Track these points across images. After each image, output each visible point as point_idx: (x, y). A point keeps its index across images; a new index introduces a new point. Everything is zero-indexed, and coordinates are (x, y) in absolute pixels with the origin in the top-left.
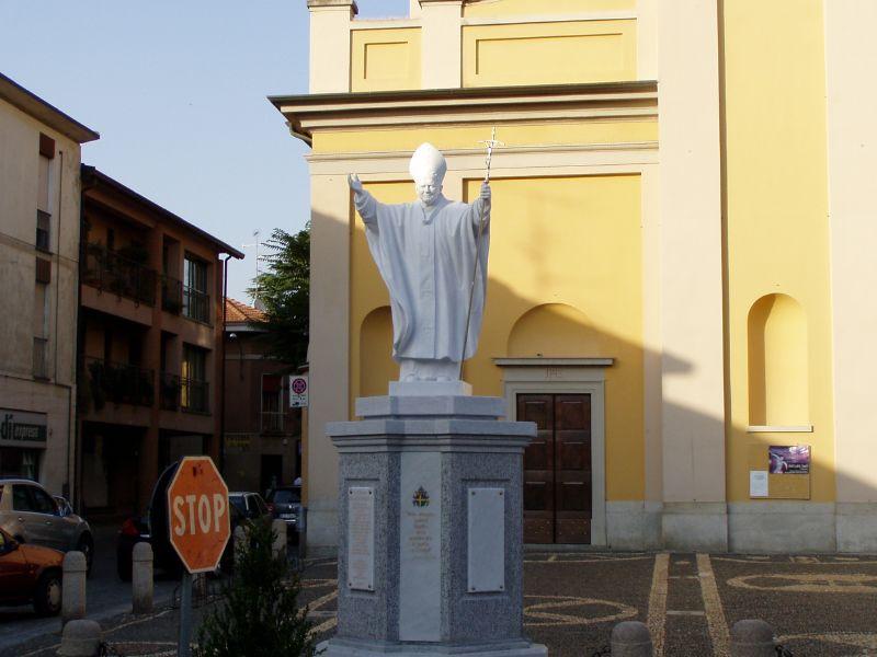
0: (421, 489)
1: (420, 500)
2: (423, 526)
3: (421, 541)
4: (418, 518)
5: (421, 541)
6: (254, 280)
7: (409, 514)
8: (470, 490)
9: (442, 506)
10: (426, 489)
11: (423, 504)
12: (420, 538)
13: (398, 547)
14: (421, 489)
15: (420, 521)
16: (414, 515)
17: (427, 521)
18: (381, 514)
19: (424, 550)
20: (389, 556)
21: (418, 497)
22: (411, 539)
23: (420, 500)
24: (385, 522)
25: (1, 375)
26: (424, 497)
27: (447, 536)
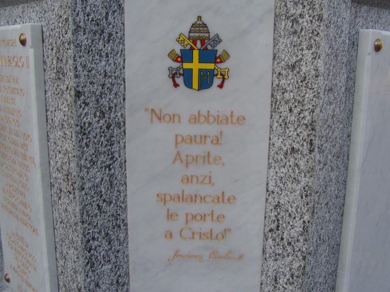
0: (199, 26)
1: (195, 66)
2: (207, 158)
3: (197, 208)
4: (186, 129)
5: (197, 208)
6: (161, 122)
7: (157, 116)
8: (369, 36)
9: (276, 89)
10: (215, 27)
11: (206, 80)
12: (193, 199)
13: (119, 222)
14: (199, 26)
15: (192, 140)
16: (173, 118)
17: (217, 141)
18: (59, 116)
19: (210, 235)
20: (90, 263)
21: (185, 56)
22: (163, 198)
23: (195, 66)
24: (69, 145)
25: (76, 1)
26: (210, 55)
27: (291, 198)
